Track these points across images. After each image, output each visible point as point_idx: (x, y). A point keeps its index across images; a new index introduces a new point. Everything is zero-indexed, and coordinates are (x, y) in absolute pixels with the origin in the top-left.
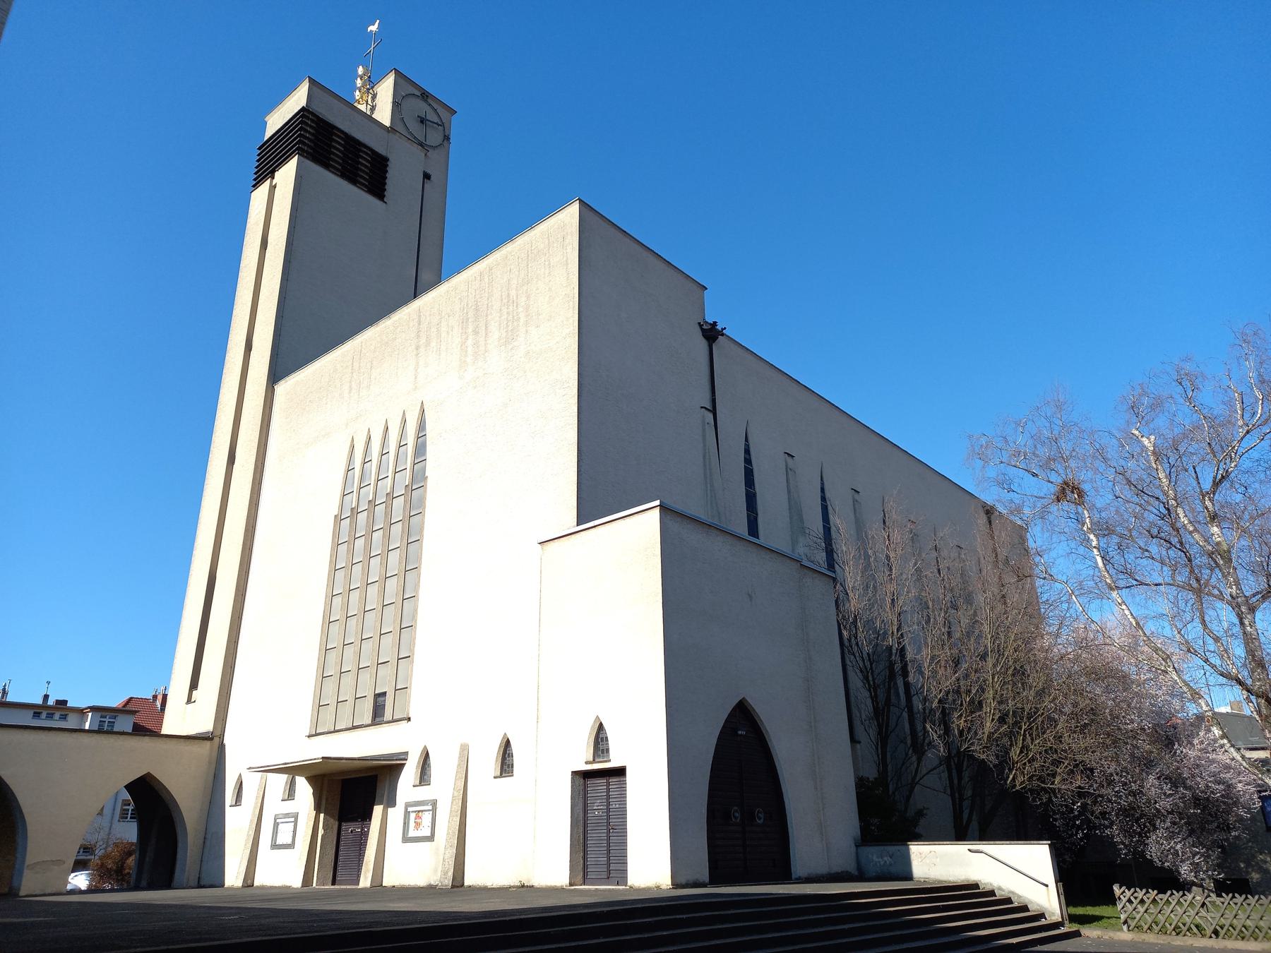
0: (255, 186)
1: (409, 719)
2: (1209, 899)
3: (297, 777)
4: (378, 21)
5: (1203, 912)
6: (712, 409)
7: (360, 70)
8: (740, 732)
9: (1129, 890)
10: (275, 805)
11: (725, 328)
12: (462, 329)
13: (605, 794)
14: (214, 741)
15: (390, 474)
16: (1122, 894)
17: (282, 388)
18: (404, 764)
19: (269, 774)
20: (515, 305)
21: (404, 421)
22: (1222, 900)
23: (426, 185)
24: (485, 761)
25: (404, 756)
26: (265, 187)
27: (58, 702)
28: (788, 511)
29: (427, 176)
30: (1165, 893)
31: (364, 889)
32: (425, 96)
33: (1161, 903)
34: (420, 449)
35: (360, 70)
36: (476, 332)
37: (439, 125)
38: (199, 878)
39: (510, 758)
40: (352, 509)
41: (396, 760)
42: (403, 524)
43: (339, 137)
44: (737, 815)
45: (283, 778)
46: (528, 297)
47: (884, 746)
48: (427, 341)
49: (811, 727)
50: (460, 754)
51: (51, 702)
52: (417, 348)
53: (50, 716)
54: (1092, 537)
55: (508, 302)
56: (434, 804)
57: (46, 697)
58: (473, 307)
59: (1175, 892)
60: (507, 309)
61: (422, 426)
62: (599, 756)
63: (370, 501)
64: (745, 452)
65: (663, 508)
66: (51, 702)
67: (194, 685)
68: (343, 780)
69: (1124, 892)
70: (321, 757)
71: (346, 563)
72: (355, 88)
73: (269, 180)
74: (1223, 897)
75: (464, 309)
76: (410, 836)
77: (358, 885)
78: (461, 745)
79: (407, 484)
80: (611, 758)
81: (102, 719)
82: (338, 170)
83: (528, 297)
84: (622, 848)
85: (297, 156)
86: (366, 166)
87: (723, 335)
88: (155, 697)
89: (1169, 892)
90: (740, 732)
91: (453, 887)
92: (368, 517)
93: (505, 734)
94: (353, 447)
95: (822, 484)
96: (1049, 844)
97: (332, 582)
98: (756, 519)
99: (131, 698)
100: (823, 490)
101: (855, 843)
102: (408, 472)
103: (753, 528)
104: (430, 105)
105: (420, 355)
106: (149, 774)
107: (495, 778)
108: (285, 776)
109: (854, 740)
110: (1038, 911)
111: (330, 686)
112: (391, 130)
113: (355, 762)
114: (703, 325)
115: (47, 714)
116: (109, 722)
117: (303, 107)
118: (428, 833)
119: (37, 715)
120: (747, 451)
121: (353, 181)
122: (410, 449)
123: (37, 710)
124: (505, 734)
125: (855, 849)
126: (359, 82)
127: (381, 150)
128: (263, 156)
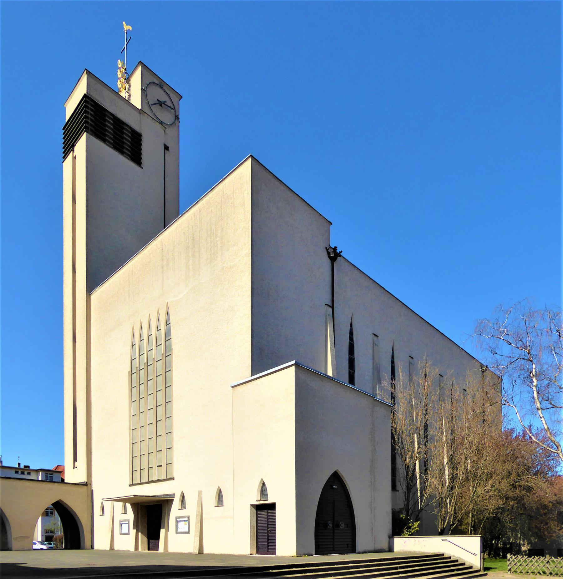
0: (65, 157)
1: (173, 479)
2: (551, 559)
3: (127, 504)
4: (124, 23)
5: (547, 565)
6: (332, 306)
7: (120, 64)
8: (334, 487)
9: (514, 556)
10: (119, 516)
11: (342, 252)
12: (186, 254)
14: (87, 484)
15: (154, 348)
16: (511, 558)
17: (94, 296)
18: (174, 499)
19: (115, 502)
20: (215, 235)
21: (159, 315)
22: (557, 559)
24: (210, 499)
25: (173, 495)
26: (70, 157)
27: (25, 467)
28: (372, 370)
29: (166, 148)
30: (531, 557)
32: (161, 84)
33: (528, 561)
34: (168, 333)
35: (120, 64)
36: (194, 256)
37: (172, 108)
43: (110, 118)
44: (330, 525)
45: (121, 504)
46: (222, 230)
47: (409, 493)
48: (167, 262)
49: (372, 484)
50: (198, 495)
51: (22, 466)
52: (162, 267)
53: (23, 473)
54: (534, 380)
55: (211, 234)
56: (188, 517)
57: (19, 464)
59: (536, 557)
60: (211, 238)
61: (168, 318)
62: (263, 497)
63: (145, 363)
64: (350, 334)
65: (296, 365)
66: (22, 466)
67: (75, 460)
69: (512, 557)
70: (133, 495)
74: (558, 558)
75: (186, 240)
76: (178, 531)
77: (158, 550)
78: (199, 491)
79: (163, 353)
80: (268, 498)
81: (47, 475)
83: (222, 230)
84: (274, 539)
85: (85, 133)
86: (128, 141)
87: (340, 256)
89: (533, 557)
90: (334, 487)
91: (199, 553)
93: (219, 486)
95: (393, 353)
96: (480, 537)
97: (131, 409)
98: (354, 373)
99: (58, 466)
100: (393, 357)
101: (389, 537)
103: (352, 380)
104: (165, 91)
105: (164, 272)
106: (60, 500)
109: (394, 487)
110: (469, 565)
111: (137, 461)
112: (141, 111)
114: (328, 249)
115: (21, 472)
116: (50, 476)
117: (85, 94)
119: (17, 472)
120: (351, 333)
121: (122, 152)
123: (17, 470)
124: (219, 486)
125: (388, 539)
126: (120, 75)
127: (136, 127)
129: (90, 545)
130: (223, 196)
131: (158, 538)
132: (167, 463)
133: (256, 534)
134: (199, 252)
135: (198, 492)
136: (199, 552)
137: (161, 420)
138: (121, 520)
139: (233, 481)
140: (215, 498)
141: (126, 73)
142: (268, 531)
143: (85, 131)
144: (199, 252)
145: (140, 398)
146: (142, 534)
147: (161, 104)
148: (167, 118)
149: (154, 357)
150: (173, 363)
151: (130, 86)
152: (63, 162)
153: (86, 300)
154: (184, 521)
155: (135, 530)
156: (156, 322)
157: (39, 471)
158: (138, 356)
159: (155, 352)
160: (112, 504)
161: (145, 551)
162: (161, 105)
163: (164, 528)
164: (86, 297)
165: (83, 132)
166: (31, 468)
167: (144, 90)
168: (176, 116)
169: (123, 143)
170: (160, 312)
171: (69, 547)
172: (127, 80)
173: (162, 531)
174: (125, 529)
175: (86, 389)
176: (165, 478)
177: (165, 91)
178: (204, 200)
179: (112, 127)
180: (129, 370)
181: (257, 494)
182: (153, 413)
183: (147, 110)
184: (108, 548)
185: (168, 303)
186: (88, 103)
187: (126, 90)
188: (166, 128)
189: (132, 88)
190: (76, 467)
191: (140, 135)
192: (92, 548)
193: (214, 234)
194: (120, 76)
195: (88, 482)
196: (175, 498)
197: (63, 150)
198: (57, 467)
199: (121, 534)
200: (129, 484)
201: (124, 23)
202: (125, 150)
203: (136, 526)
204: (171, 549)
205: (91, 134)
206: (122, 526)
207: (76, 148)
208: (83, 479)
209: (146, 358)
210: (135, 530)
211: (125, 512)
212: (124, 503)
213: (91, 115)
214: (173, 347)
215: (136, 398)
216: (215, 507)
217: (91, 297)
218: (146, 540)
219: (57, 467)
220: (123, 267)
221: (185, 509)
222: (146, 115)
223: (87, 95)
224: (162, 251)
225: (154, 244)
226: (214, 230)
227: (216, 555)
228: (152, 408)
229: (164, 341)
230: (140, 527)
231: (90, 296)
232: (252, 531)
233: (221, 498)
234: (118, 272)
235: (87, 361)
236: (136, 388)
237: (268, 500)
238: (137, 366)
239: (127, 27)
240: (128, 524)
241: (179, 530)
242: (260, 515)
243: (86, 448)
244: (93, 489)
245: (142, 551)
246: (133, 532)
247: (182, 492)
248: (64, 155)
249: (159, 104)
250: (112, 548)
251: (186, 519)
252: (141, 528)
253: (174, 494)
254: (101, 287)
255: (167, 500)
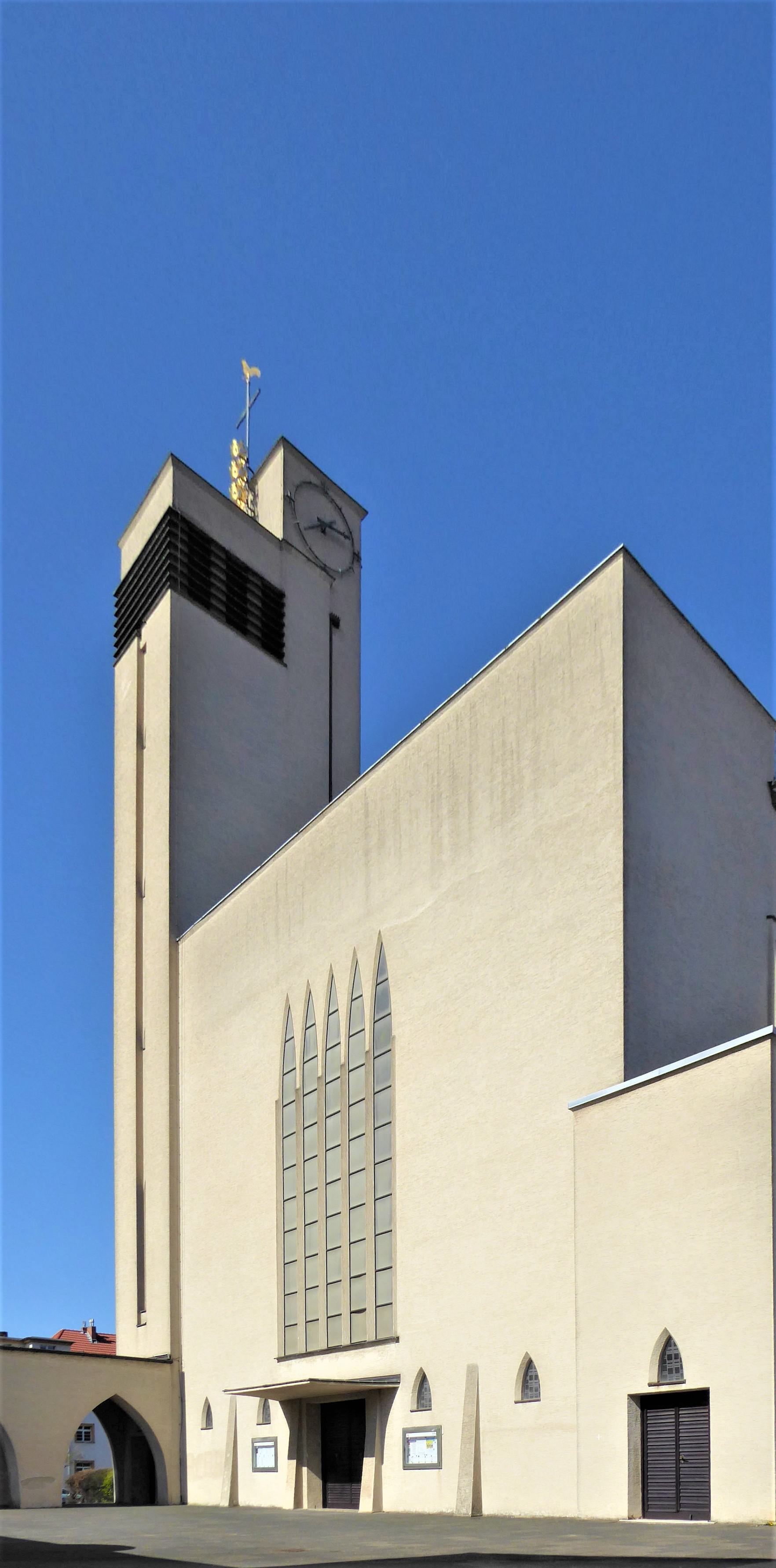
0: (118, 655)
3: (270, 1401)
4: (244, 363)
7: (235, 450)
12: (432, 811)
13: (674, 1428)
15: (343, 1039)
17: (188, 944)
20: (515, 756)
23: (333, 637)
25: (396, 1379)
26: (131, 653)
29: (335, 622)
31: (365, 1516)
34: (382, 1001)
35: (235, 450)
37: (346, 537)
38: (181, 1497)
39: (428, 1393)
40: (297, 1090)
41: (388, 1383)
42: (366, 1103)
45: (256, 1401)
52: (367, 852)
56: (438, 1429)
58: (448, 774)
60: (503, 766)
61: (381, 968)
63: (319, 1078)
67: (141, 1308)
68: (322, 1405)
70: (307, 1378)
71: (297, 1158)
72: (229, 480)
73: (136, 640)
76: (410, 1463)
78: (469, 1367)
79: (367, 1049)
82: (221, 611)
85: (169, 592)
88: (85, 1329)
92: (296, 1109)
93: (527, 1353)
94: (289, 1009)
97: (282, 1185)
99: (64, 1330)
102: (368, 1034)
104: (332, 501)
106: (116, 1396)
107: (412, 1411)
108: (258, 1399)
112: (284, 544)
113: (344, 1384)
118: (435, 1461)
122: (368, 1001)
126: (235, 472)
127: (274, 579)
128: (124, 604)
129: (179, 1495)
130: (540, 659)
131: (355, 1476)
132: (307, 1320)
133: (640, 1468)
134: (470, 801)
135: (466, 1368)
136: (472, 1514)
137: (364, 1204)
138: (255, 1439)
139: (576, 1338)
140: (517, 1381)
141: (249, 468)
142: (678, 1461)
143: (170, 587)
144: (470, 801)
145: (305, 1159)
146: (310, 1471)
147: (323, 527)
148: (338, 559)
149: (343, 1061)
150: (396, 1070)
151: (255, 496)
152: (114, 666)
153: (168, 952)
154: (427, 1438)
155: (294, 1462)
156: (348, 979)
157: (28, 1341)
158: (300, 1063)
159: (345, 1051)
160: (231, 1401)
161: (316, 1510)
162: (323, 532)
163: (372, 1456)
164: (168, 947)
165: (164, 590)
166: (10, 1336)
167: (290, 499)
168: (354, 553)
169: (247, 611)
170: (359, 956)
171: (127, 1499)
172: (251, 485)
173: (368, 1464)
174: (265, 1458)
175: (168, 1150)
176: (374, 1339)
177: (332, 501)
178: (483, 680)
179: (223, 577)
180: (276, 1096)
181: (650, 1368)
182: (342, 1190)
183: (296, 541)
184: (225, 1503)
185: (382, 933)
186: (175, 525)
187: (247, 504)
188: (335, 579)
189: (260, 500)
190: (142, 1323)
191: (281, 595)
192: (183, 1501)
193: (512, 755)
194: (235, 475)
195: (174, 1357)
196: (400, 1386)
197: (116, 640)
198: (61, 1334)
199: (256, 1470)
200: (277, 1357)
201: (244, 363)
202: (249, 627)
203: (295, 1452)
204: (389, 1505)
205: (181, 594)
206: (257, 1453)
207: (144, 630)
208: (162, 1348)
209: (322, 1067)
210: (295, 1460)
211: (266, 1418)
212: (263, 1400)
213: (182, 551)
214: (394, 1033)
215: (340, 1141)
216: (516, 1402)
217: (180, 947)
218: (318, 1482)
219: (61, 1334)
220: (261, 868)
221: (270, 1423)
222: (293, 551)
223: (174, 509)
224: (367, 816)
225: (343, 804)
226: (511, 743)
227: (520, 1519)
228: (340, 1179)
229: (370, 1022)
230: (306, 1455)
231: (178, 945)
232: (633, 1460)
233: (529, 1381)
234: (249, 880)
235: (171, 1088)
236: (297, 1135)
237: (684, 1382)
238: (298, 1086)
239: (249, 372)
240: (273, 1449)
241: (413, 1460)
242: (653, 1422)
243: (168, 1281)
244: (184, 1370)
245: (310, 1509)
246: (287, 1466)
247: (421, 1370)
248: (116, 650)
249: (320, 529)
250: (234, 1502)
251: (433, 1434)
252: (307, 1456)
253: (398, 1376)
254: (205, 922)
255: (380, 1391)
